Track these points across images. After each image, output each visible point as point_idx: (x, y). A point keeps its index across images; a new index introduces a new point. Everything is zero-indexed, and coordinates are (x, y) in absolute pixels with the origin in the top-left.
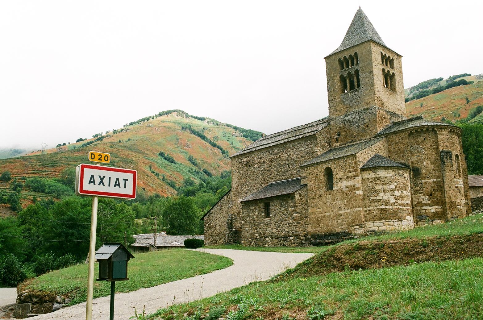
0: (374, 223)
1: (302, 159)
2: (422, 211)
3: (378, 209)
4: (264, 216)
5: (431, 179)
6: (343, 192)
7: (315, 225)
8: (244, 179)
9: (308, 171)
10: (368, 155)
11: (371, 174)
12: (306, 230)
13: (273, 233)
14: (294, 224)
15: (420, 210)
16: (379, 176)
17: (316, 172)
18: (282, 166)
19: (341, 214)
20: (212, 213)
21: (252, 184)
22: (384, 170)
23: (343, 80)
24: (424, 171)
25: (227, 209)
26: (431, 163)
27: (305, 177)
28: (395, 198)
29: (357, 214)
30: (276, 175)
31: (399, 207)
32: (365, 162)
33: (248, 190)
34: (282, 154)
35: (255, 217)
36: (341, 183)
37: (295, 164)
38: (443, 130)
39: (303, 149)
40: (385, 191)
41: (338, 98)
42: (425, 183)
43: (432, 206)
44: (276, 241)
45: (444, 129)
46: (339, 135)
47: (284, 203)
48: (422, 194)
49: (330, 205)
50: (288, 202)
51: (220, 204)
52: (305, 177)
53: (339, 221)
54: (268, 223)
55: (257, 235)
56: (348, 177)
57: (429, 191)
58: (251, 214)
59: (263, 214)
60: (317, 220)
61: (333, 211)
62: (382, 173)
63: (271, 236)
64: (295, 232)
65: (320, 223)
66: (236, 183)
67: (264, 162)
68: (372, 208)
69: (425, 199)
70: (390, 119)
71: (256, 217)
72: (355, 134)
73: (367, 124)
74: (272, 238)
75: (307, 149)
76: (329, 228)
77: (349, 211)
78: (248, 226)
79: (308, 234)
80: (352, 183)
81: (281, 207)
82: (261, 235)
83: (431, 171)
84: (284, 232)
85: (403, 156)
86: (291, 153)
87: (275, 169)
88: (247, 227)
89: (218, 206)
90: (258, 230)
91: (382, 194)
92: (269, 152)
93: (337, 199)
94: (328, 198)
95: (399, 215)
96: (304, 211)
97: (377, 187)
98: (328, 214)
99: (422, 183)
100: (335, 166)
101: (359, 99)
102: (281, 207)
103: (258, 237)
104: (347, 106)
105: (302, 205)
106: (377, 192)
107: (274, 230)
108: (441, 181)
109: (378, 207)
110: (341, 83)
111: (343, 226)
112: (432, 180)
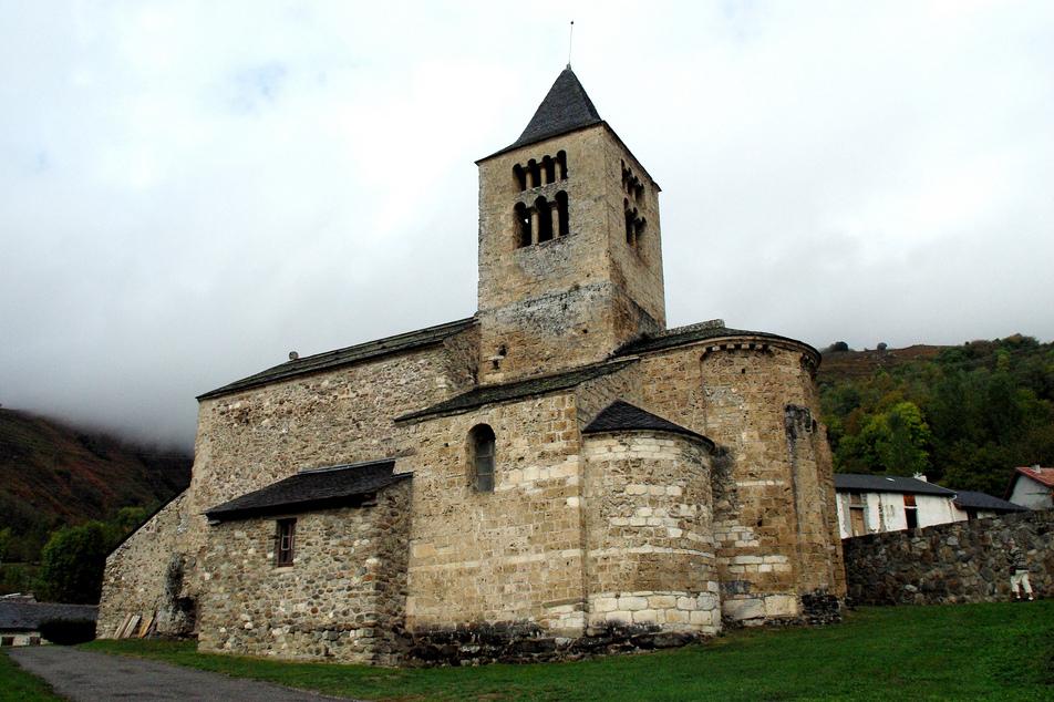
0: (618, 596)
1: (399, 407)
2: (734, 570)
3: (634, 556)
4: (274, 560)
5: (760, 479)
6: (525, 500)
7: (430, 598)
8: (227, 458)
9: (418, 435)
10: (601, 397)
11: (614, 449)
12: (400, 610)
13: (296, 615)
14: (366, 590)
15: (730, 565)
16: (640, 457)
17: (444, 439)
18: (340, 425)
19: (515, 566)
20: (128, 548)
21: (248, 471)
22: (653, 440)
23: (521, 211)
24: (741, 458)
25: (170, 540)
26: (761, 437)
27: (409, 453)
28: (681, 526)
29: (566, 569)
30: (320, 448)
31: (691, 552)
32: (594, 415)
33: (237, 488)
34: (344, 393)
35: (246, 561)
36: (520, 472)
37: (376, 422)
38: (788, 352)
39: (403, 381)
40: (654, 502)
41: (506, 260)
42: (746, 490)
43: (762, 555)
44: (304, 639)
45: (791, 351)
46: (503, 353)
47: (341, 525)
48: (735, 522)
49: (482, 538)
50: (351, 522)
51: (154, 523)
52: (409, 453)
53: (508, 588)
54: (283, 583)
55: (245, 617)
56: (543, 455)
57: (756, 512)
58: (234, 553)
59: (270, 555)
60: (437, 584)
61: (490, 555)
62: (647, 447)
63: (290, 623)
64: (367, 615)
65: (446, 590)
66: (206, 467)
67: (290, 412)
68: (613, 551)
69: (746, 536)
70: (639, 324)
71: (250, 563)
72: (548, 353)
73: (584, 327)
74: (292, 632)
75: (413, 380)
76: (474, 609)
77: (541, 557)
78: (221, 589)
79: (404, 623)
80: (555, 472)
81: (329, 534)
82: (258, 618)
83: (761, 459)
84: (331, 615)
85: (684, 413)
86: (368, 389)
87: (318, 433)
88: (217, 592)
89: (148, 529)
90: (250, 603)
91: (645, 511)
92: (308, 387)
93: (505, 521)
94: (474, 515)
95: (691, 577)
96: (399, 553)
97: (632, 489)
98: (473, 564)
99: (735, 491)
100: (504, 421)
101: (563, 264)
102: (329, 534)
103: (249, 625)
104: (529, 279)
105: (394, 532)
106: (631, 504)
107: (300, 605)
108: (787, 485)
109: (633, 550)
110: (516, 223)
111: (520, 605)
112: (762, 483)
